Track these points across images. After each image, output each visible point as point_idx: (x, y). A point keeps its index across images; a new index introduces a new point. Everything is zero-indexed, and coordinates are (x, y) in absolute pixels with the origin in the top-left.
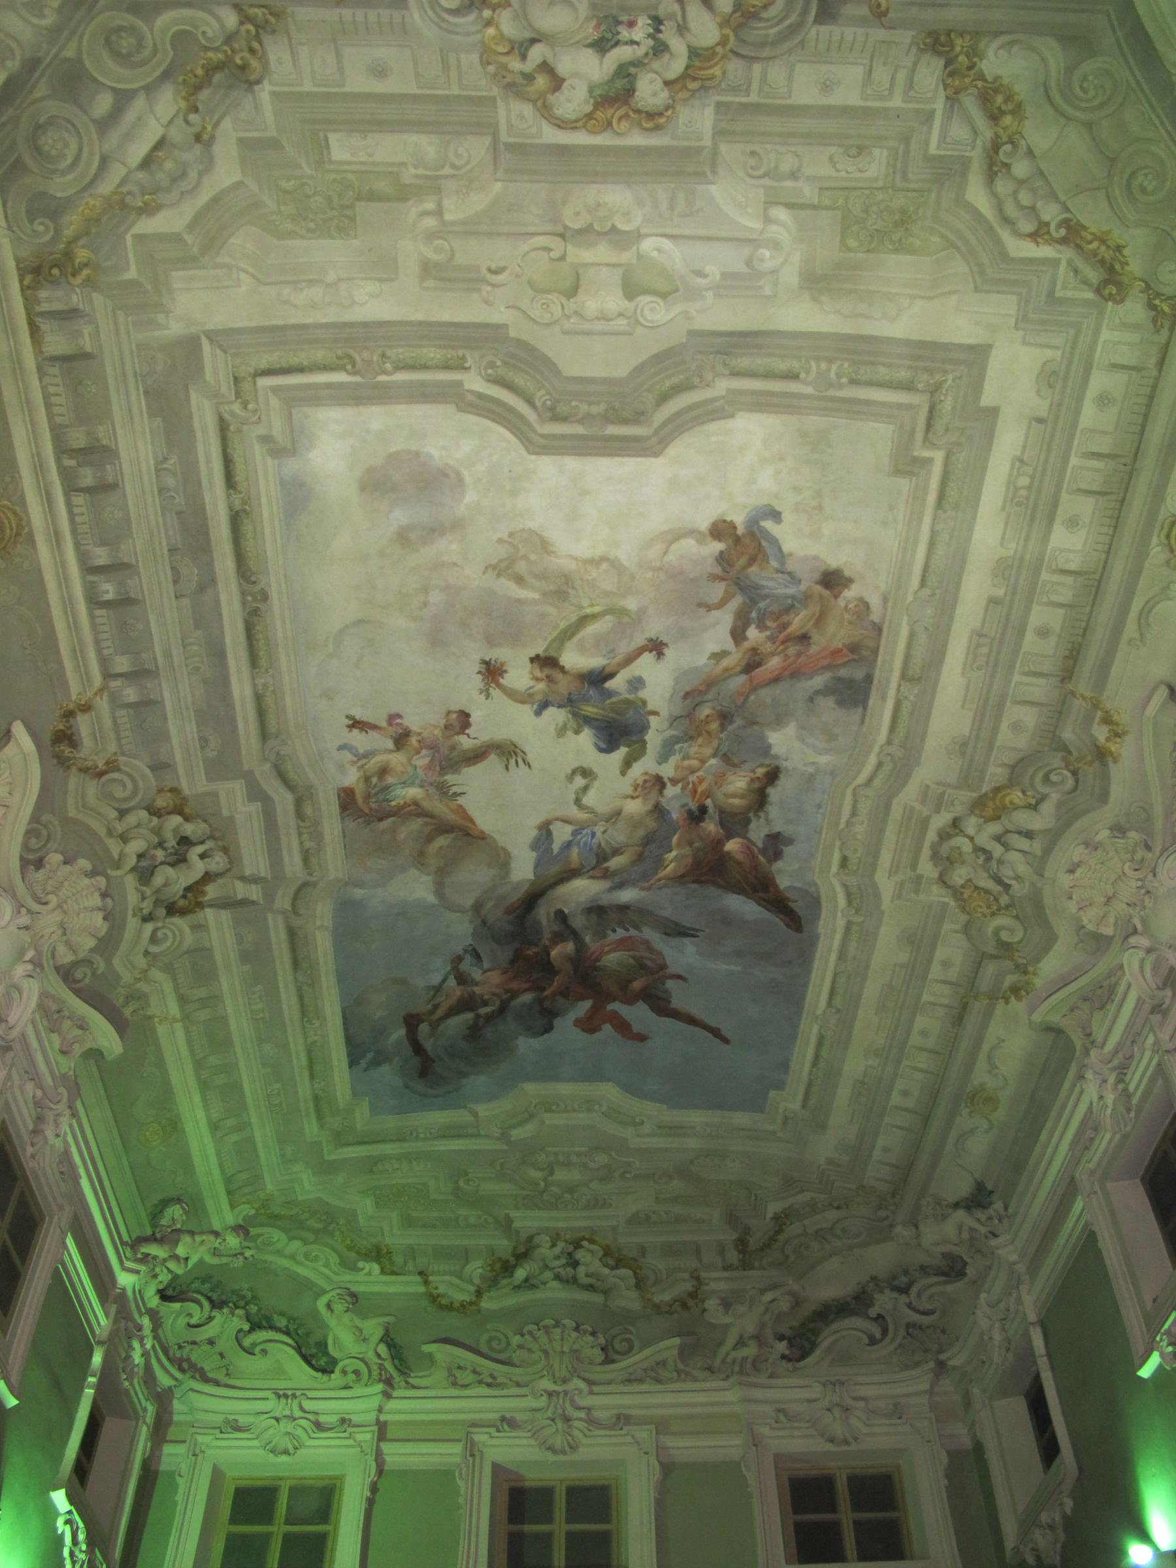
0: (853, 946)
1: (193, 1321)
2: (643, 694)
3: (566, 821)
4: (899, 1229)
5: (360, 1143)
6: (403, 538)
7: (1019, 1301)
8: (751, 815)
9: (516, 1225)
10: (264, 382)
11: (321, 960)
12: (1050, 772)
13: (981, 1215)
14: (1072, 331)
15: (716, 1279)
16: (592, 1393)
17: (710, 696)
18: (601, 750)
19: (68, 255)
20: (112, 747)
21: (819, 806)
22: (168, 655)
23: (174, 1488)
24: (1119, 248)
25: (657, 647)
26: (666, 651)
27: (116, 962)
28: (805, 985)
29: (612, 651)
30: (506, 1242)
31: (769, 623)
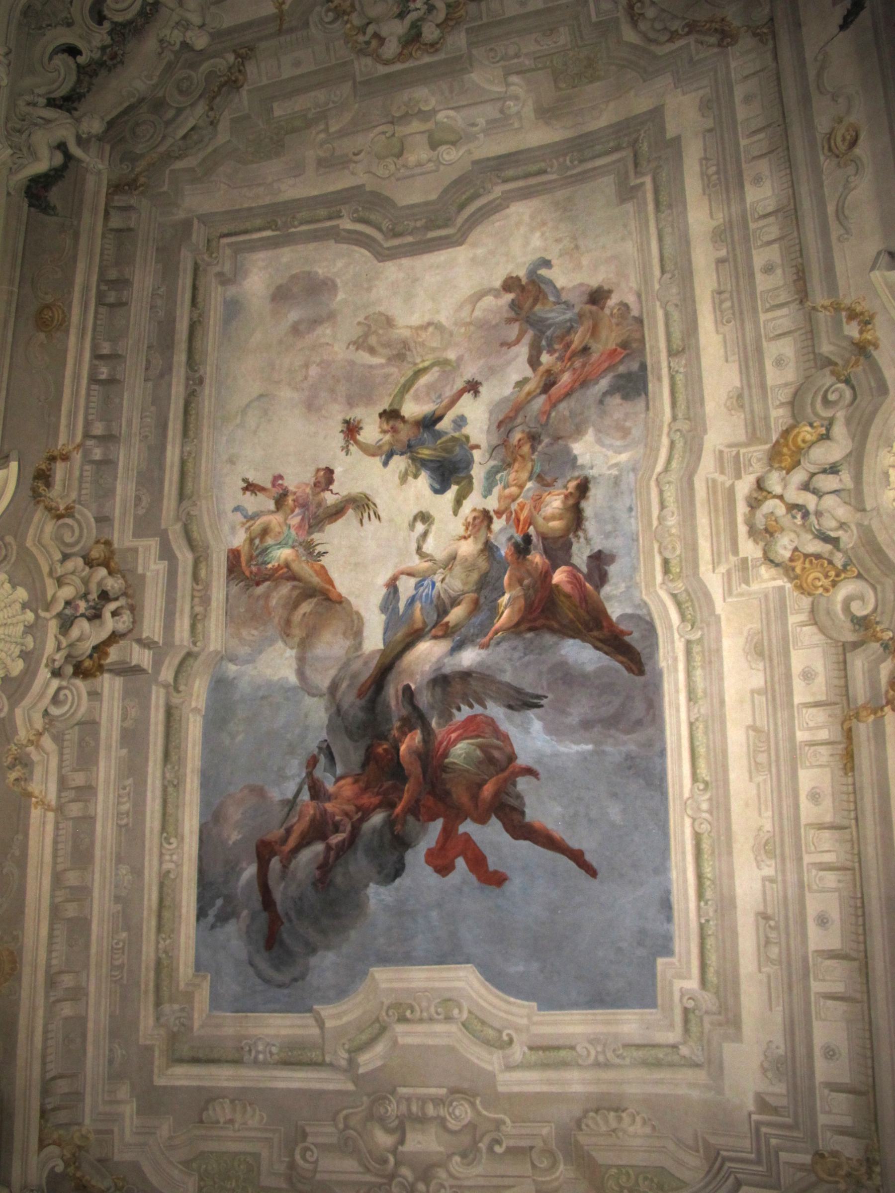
2: (466, 430)
3: (410, 574)
6: (296, 330)
8: (571, 536)
10: (225, 241)
12: (826, 391)
14: (712, 74)
17: (519, 420)
18: (436, 492)
19: (135, 180)
21: (630, 509)
24: (723, 20)
25: (473, 387)
26: (481, 389)
27: (18, 712)
28: (663, 753)
29: (440, 396)
31: (556, 347)
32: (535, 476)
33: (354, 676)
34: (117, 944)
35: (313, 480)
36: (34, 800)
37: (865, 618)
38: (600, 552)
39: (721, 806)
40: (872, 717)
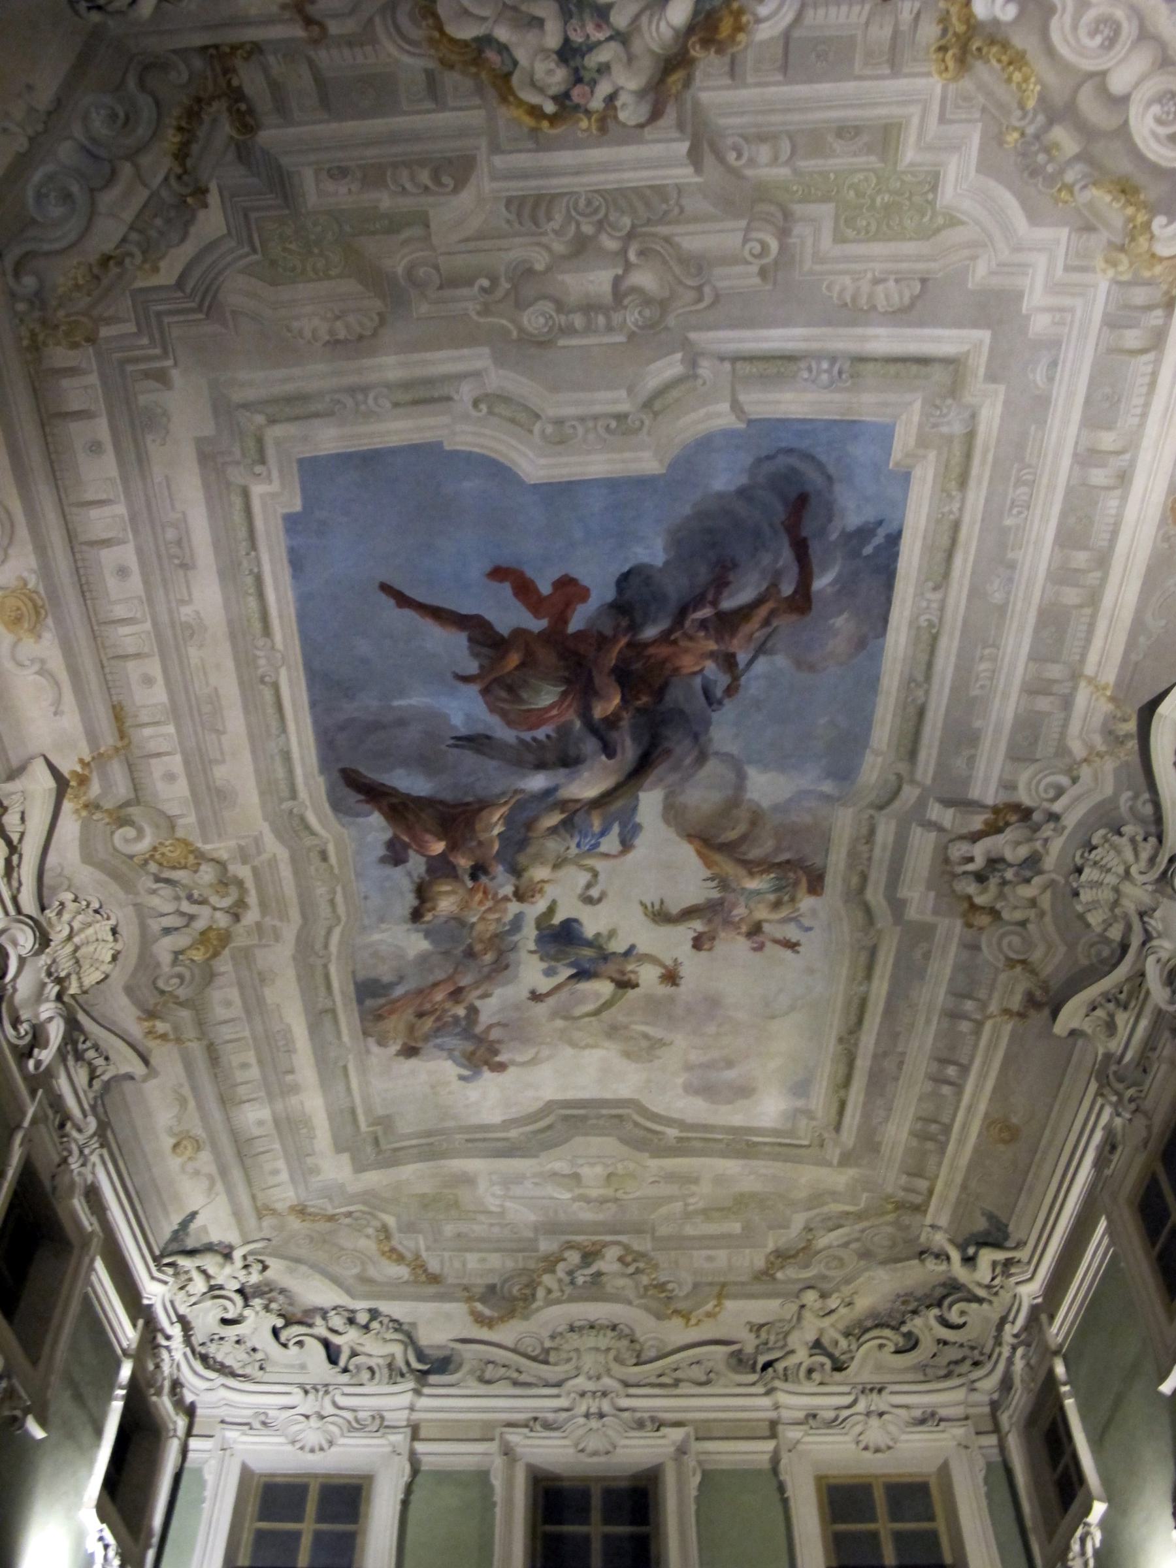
0: (281, 773)
3: (606, 856)
5: (923, 361)
6: (730, 1064)
9: (684, 147)
10: (806, 1143)
16: (628, 1396)
17: (486, 970)
18: (576, 921)
22: (928, 1021)
25: (535, 997)
27: (1109, 790)
28: (313, 704)
30: (705, 97)
33: (675, 768)
34: (1020, 513)
35: (716, 942)
36: (1108, 693)
37: (121, 826)
39: (244, 661)
40: (102, 750)
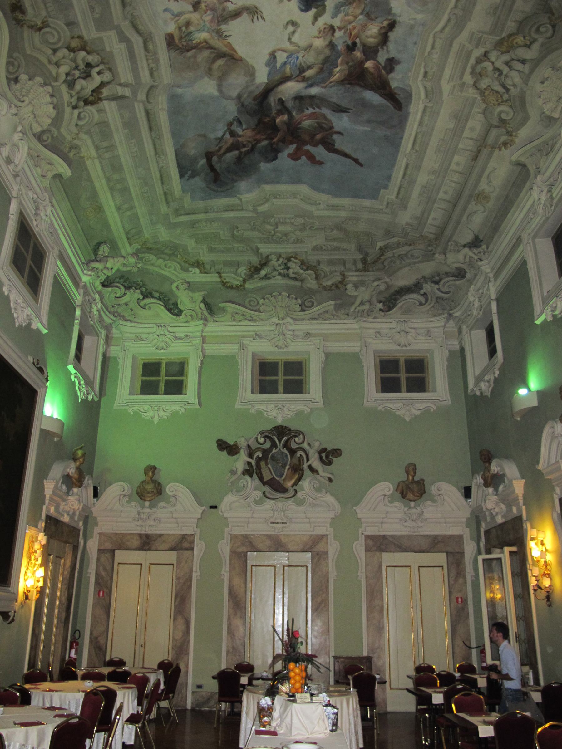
0: (426, 119)
1: (117, 296)
3: (284, 51)
4: (437, 255)
5: (187, 214)
7: (488, 290)
9: (260, 251)
11: (163, 124)
13: (476, 251)
15: (352, 276)
18: (302, 11)
20: (44, 13)
21: (415, 43)
23: (117, 363)
27: (62, 130)
28: (401, 138)
32: (365, 13)
33: (251, 92)
36: (85, 158)
37: (505, 120)
38: (393, 58)
